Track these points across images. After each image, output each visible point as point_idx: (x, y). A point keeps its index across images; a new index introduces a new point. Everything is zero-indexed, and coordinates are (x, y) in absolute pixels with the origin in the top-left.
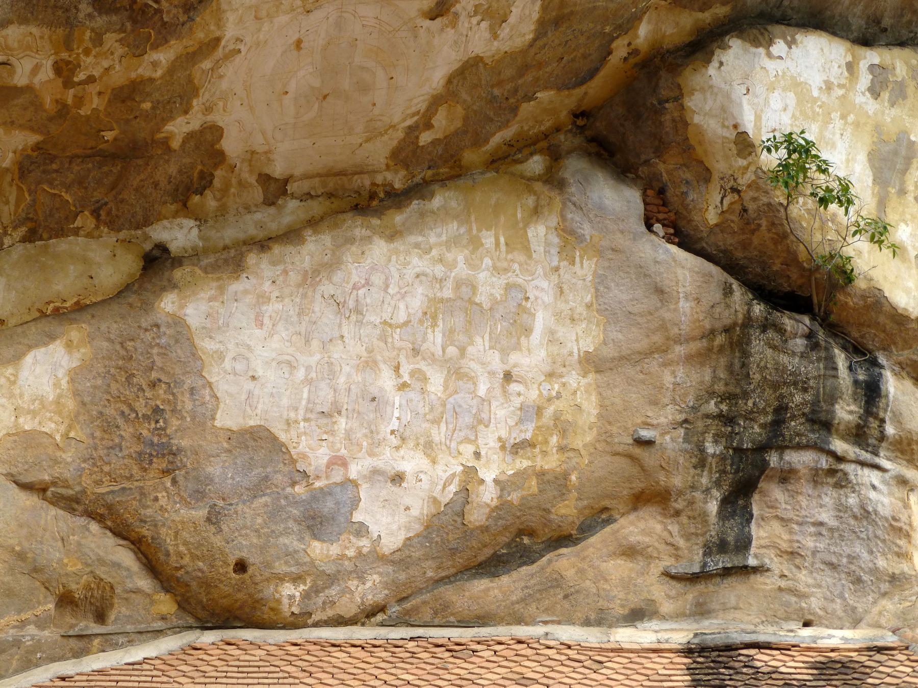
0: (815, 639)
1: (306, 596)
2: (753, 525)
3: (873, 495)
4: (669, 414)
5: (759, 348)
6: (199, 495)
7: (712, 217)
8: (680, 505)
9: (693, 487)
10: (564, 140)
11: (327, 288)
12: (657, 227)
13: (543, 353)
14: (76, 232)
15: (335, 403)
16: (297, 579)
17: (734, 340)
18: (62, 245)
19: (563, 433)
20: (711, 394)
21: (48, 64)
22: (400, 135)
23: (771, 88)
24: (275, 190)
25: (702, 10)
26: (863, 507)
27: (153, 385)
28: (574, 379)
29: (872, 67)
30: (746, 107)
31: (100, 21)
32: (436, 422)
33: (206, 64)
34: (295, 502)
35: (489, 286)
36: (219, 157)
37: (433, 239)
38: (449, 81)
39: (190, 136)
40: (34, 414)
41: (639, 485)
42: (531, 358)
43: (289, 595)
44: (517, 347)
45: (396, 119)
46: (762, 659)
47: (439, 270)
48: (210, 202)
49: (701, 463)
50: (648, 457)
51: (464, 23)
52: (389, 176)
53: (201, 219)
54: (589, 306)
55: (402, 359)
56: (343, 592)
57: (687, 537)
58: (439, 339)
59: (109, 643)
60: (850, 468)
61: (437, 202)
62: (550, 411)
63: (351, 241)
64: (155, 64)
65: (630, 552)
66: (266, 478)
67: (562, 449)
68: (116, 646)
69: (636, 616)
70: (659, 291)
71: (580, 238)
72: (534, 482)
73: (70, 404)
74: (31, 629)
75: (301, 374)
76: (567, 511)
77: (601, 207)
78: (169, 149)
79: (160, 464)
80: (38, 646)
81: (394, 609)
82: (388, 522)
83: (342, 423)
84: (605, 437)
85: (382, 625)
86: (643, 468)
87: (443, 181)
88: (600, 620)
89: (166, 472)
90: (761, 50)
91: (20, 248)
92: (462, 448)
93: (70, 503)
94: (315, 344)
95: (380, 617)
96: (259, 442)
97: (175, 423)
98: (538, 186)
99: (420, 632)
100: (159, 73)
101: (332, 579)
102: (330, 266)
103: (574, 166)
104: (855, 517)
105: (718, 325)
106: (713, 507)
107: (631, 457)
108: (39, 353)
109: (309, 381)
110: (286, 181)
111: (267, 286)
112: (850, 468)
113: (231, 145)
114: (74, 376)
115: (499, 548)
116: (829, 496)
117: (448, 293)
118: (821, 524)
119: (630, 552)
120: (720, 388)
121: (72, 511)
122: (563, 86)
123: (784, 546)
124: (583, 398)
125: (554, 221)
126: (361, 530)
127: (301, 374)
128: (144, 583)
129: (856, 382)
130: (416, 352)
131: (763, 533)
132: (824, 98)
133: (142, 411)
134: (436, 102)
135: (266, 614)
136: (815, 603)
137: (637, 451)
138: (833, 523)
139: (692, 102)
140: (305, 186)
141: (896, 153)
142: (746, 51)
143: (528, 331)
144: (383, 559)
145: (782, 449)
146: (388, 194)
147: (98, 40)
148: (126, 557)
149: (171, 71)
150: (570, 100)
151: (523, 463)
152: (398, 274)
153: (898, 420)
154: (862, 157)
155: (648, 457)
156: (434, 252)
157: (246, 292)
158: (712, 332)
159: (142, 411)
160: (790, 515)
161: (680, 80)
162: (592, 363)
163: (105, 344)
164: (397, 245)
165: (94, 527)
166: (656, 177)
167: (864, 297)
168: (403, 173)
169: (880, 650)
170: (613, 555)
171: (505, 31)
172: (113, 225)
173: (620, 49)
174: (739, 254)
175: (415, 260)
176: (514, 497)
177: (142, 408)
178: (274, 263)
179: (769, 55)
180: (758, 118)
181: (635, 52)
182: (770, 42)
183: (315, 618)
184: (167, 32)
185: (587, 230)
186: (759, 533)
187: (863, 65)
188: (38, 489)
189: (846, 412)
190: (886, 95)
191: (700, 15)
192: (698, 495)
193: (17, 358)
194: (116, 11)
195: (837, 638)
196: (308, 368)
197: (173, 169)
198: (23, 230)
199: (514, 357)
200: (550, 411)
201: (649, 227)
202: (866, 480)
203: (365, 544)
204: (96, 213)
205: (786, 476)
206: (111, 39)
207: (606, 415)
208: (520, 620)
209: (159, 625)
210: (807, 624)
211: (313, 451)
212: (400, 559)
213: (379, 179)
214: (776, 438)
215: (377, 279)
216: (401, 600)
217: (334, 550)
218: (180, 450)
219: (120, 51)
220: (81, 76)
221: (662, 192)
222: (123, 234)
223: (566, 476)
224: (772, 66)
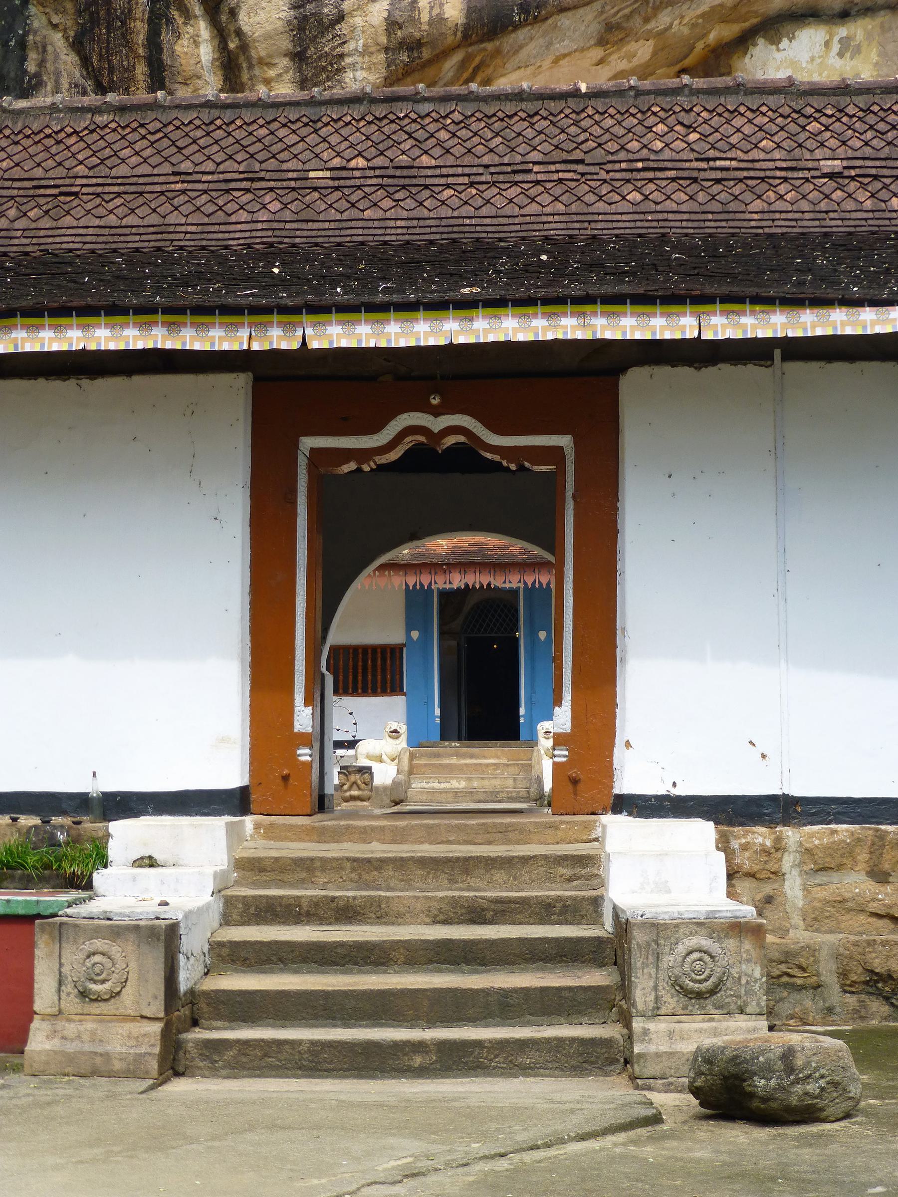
25: (744, 22)
51: (613, 63)
90: (774, 47)
132: (809, 66)
142: (766, 47)
161: (731, 63)
179: (778, 50)
182: (780, 41)
187: (836, 39)
190: (848, 55)
224: (779, 56)
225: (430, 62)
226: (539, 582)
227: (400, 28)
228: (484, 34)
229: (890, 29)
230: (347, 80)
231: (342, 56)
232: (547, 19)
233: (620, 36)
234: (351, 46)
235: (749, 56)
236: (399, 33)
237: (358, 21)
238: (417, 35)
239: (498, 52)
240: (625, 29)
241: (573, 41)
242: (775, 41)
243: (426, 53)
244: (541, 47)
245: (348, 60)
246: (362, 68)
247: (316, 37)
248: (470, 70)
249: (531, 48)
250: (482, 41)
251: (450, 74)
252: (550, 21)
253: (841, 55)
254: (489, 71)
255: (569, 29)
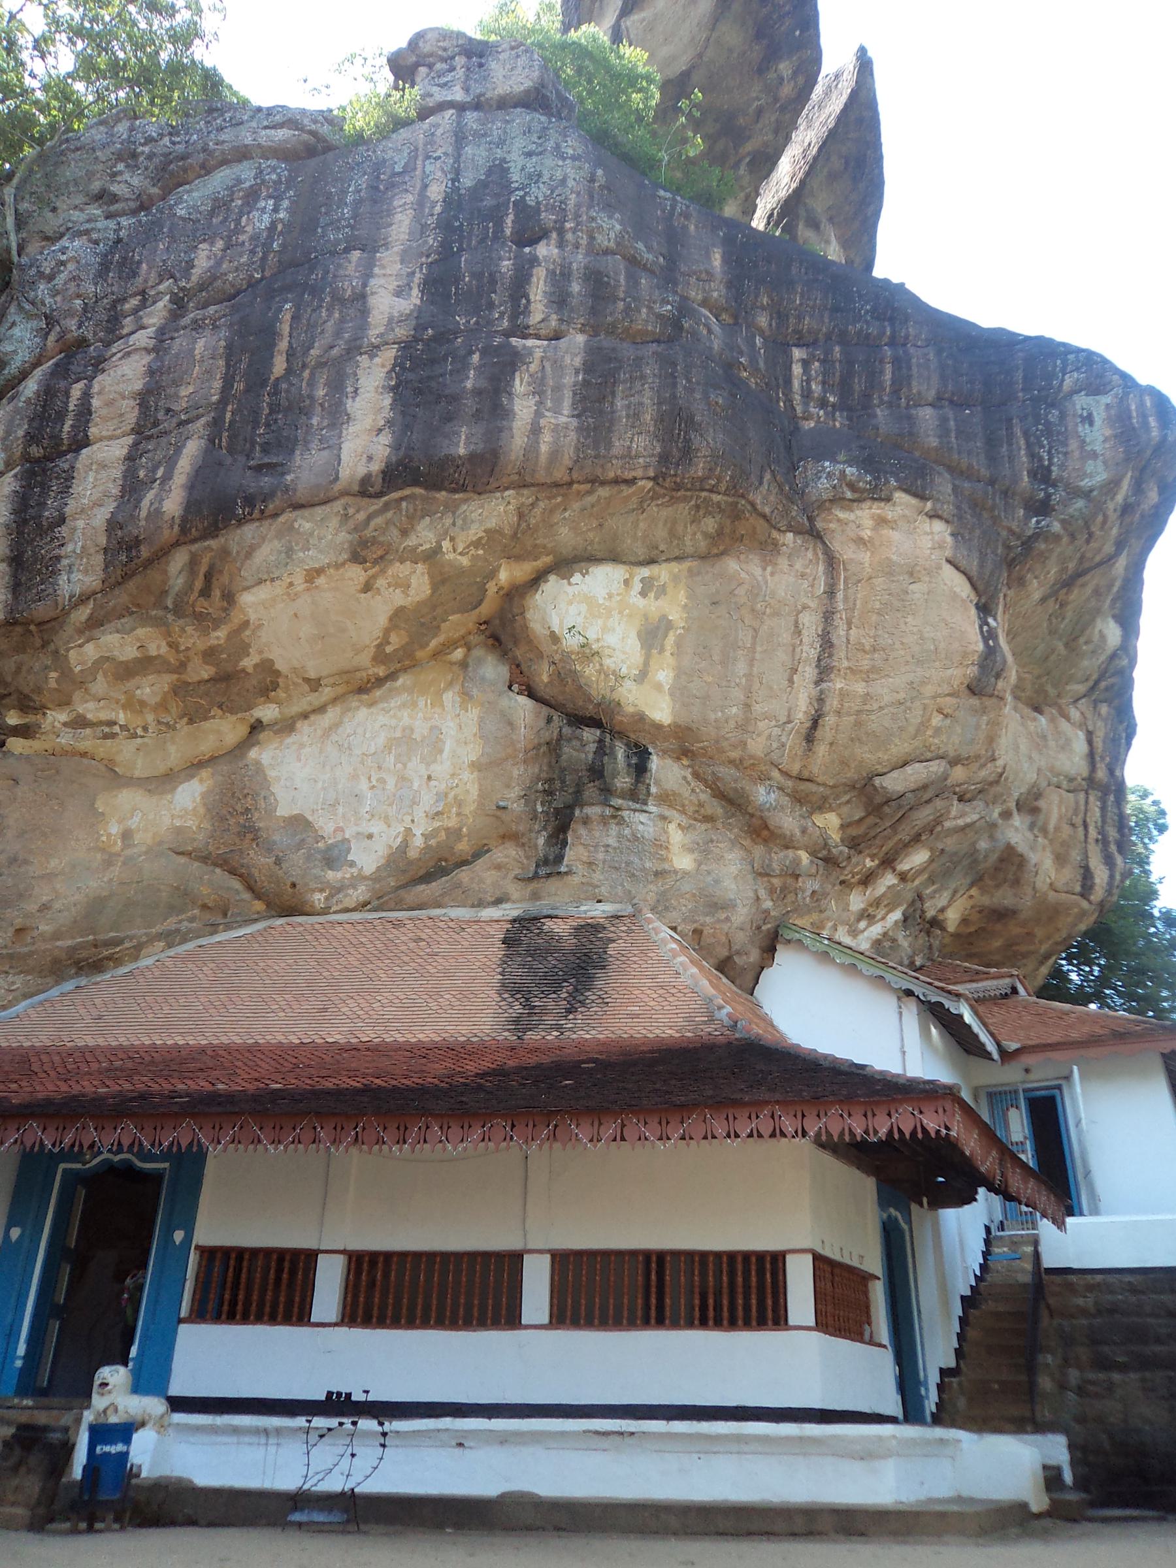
0: (585, 912)
1: (327, 899)
2: (567, 848)
3: (641, 827)
4: (516, 792)
5: (567, 751)
6: (269, 850)
7: (545, 678)
8: (525, 840)
9: (530, 831)
10: (474, 639)
11: (334, 737)
12: (515, 687)
13: (449, 763)
14: (214, 717)
15: (336, 799)
16: (322, 890)
17: (553, 748)
18: (206, 725)
19: (460, 806)
20: (539, 779)
21: (164, 643)
22: (373, 650)
23: (570, 603)
24: (315, 684)
26: (634, 835)
27: (245, 796)
28: (467, 776)
29: (642, 580)
30: (554, 616)
31: (181, 622)
32: (390, 805)
33: (248, 633)
34: (319, 851)
35: (421, 728)
36: (277, 673)
37: (392, 705)
38: (391, 619)
39: (256, 666)
40: (181, 817)
41: (501, 831)
42: (442, 768)
43: (318, 899)
44: (435, 761)
45: (368, 642)
46: (549, 924)
47: (393, 722)
48: (281, 694)
49: (535, 818)
50: (505, 816)
52: (376, 670)
53: (279, 703)
54: (475, 735)
55: (373, 773)
56: (346, 895)
57: (527, 858)
58: (392, 761)
59: (228, 927)
60: (625, 814)
61: (400, 681)
62: (451, 795)
63: (349, 710)
64: (218, 638)
65: (498, 867)
66: (303, 840)
67: (458, 814)
68: (231, 929)
69: (498, 902)
70: (510, 724)
71: (471, 697)
72: (443, 833)
73: (202, 811)
74: (185, 923)
75: (320, 785)
76: (463, 847)
77: (483, 679)
78: (248, 674)
79: (249, 836)
80: (189, 931)
81: (375, 903)
82: (367, 859)
83: (340, 810)
84: (481, 805)
85: (369, 911)
86: (503, 822)
87: (405, 670)
88: (480, 904)
89: (253, 840)
90: (565, 581)
91: (186, 728)
92: (405, 818)
93: (205, 859)
94: (328, 768)
95: (369, 907)
96: (299, 823)
97: (256, 815)
98: (455, 668)
99: (384, 914)
100: (222, 642)
101: (339, 890)
102: (336, 726)
103: (478, 652)
104: (629, 841)
105: (542, 741)
106: (541, 841)
107: (497, 817)
108: (185, 785)
109: (324, 789)
110: (319, 680)
111: (305, 738)
112: (625, 814)
113: (280, 665)
114: (204, 796)
115: (426, 873)
116: (614, 829)
117: (398, 734)
118: (608, 846)
119: (498, 867)
120: (544, 775)
121: (206, 863)
122: (463, 610)
123: (585, 859)
124: (470, 786)
125: (457, 688)
126: (352, 864)
127: (320, 785)
128: (247, 896)
129: (629, 765)
130: (380, 768)
131: (573, 855)
133: (240, 810)
134: (387, 632)
135: (307, 909)
136: (604, 891)
137: (499, 813)
138: (616, 845)
139: (528, 616)
140: (331, 680)
141: (658, 628)
143: (441, 751)
144: (365, 878)
145: (582, 806)
146: (377, 679)
147: (183, 630)
148: (236, 884)
149: (229, 638)
150: (473, 616)
151: (437, 824)
152: (371, 725)
153: (657, 783)
154: (633, 634)
155: (505, 816)
156: (392, 712)
157: (294, 743)
158: (540, 745)
159: (240, 810)
160: (589, 842)
162: (475, 766)
163: (221, 778)
164: (373, 710)
165: (218, 870)
166: (515, 658)
167: (633, 716)
168: (383, 667)
169: (618, 917)
170: (489, 869)
171: (412, 592)
172: (232, 711)
173: (492, 588)
174: (561, 698)
175: (381, 718)
176: (433, 842)
177: (239, 808)
178: (310, 726)
179: (570, 584)
180: (561, 622)
181: (501, 588)
182: (572, 575)
183: (334, 909)
184: (217, 624)
185: (475, 692)
186: (570, 854)
187: (637, 579)
188: (188, 854)
189: (623, 781)
190: (652, 595)
191: (534, 563)
192: (533, 835)
193: (175, 788)
194: (187, 616)
195: (597, 911)
196: (324, 782)
197: (254, 682)
198: (186, 719)
199: (433, 767)
200: (451, 795)
201: (510, 687)
202: (636, 820)
203: (354, 870)
204: (220, 707)
205: (586, 821)
206: (189, 629)
207: (483, 795)
208: (439, 906)
209: (256, 916)
210: (599, 901)
211: (326, 825)
212: (375, 878)
213: (370, 672)
214: (578, 800)
215: (360, 730)
216: (379, 898)
217: (339, 875)
218: (259, 829)
219: (196, 634)
220: (183, 648)
221: (518, 666)
222: (239, 716)
223: (460, 829)
224: (570, 590)
225: (149, 563)
226: (827, 1132)
227: (121, 528)
228: (205, 529)
229: (699, 573)
230: (61, 582)
231: (58, 558)
232: (275, 515)
233: (380, 553)
234: (69, 548)
235: (540, 592)
236: (119, 533)
237: (80, 524)
238: (135, 532)
239: (225, 552)
240: (381, 544)
241: (321, 552)
242: (567, 576)
243: (145, 552)
244: (280, 552)
245: (65, 562)
246: (79, 570)
247: (33, 540)
248: (201, 576)
249: (267, 552)
250: (203, 537)
251: (180, 581)
252: (282, 519)
253: (643, 594)
254: (225, 579)
255: (311, 534)
